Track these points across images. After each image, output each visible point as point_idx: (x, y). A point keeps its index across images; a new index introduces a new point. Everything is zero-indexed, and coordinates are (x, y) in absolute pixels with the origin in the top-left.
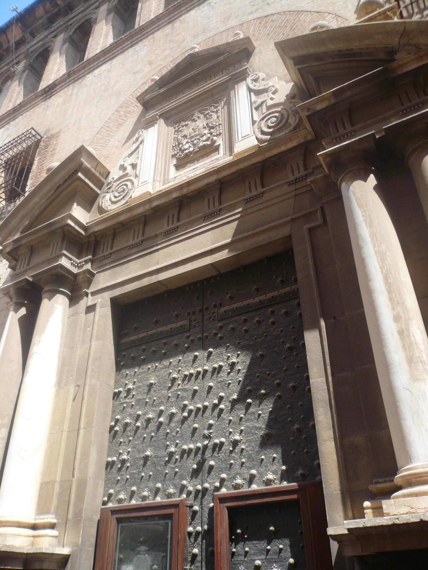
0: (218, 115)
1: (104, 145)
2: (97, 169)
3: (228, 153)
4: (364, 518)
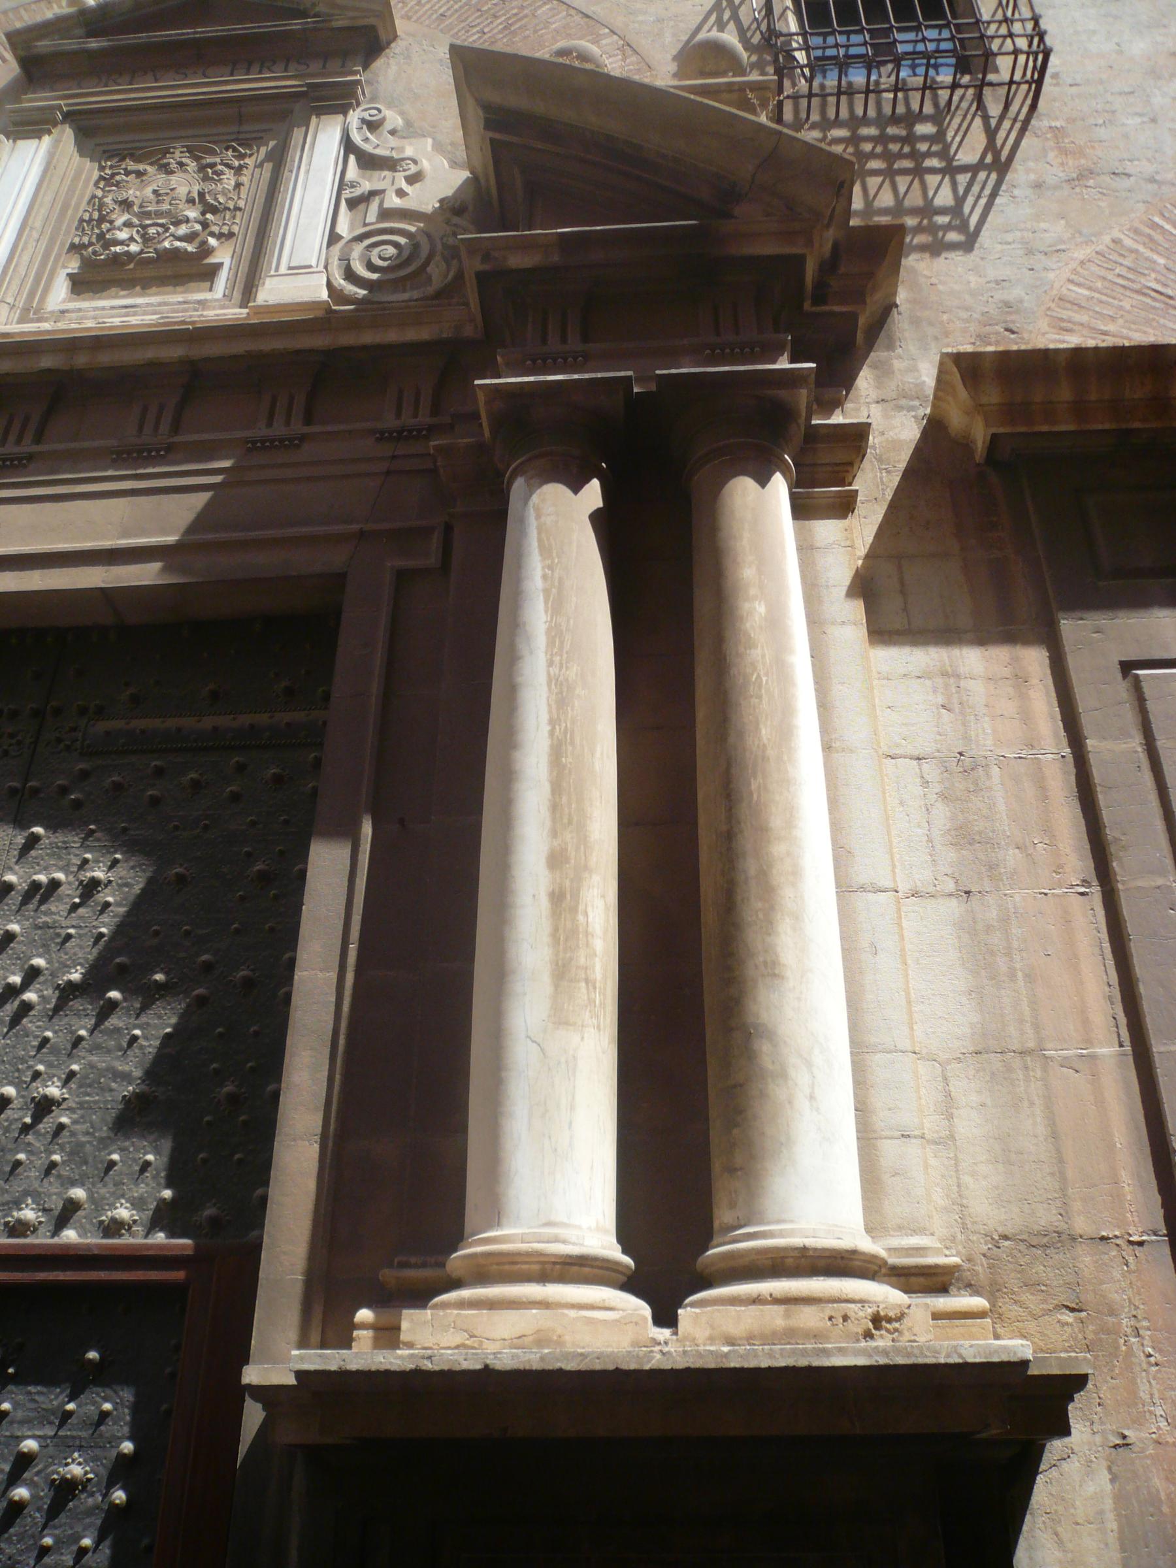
0: (239, 180)
3: (237, 296)
4: (350, 1348)
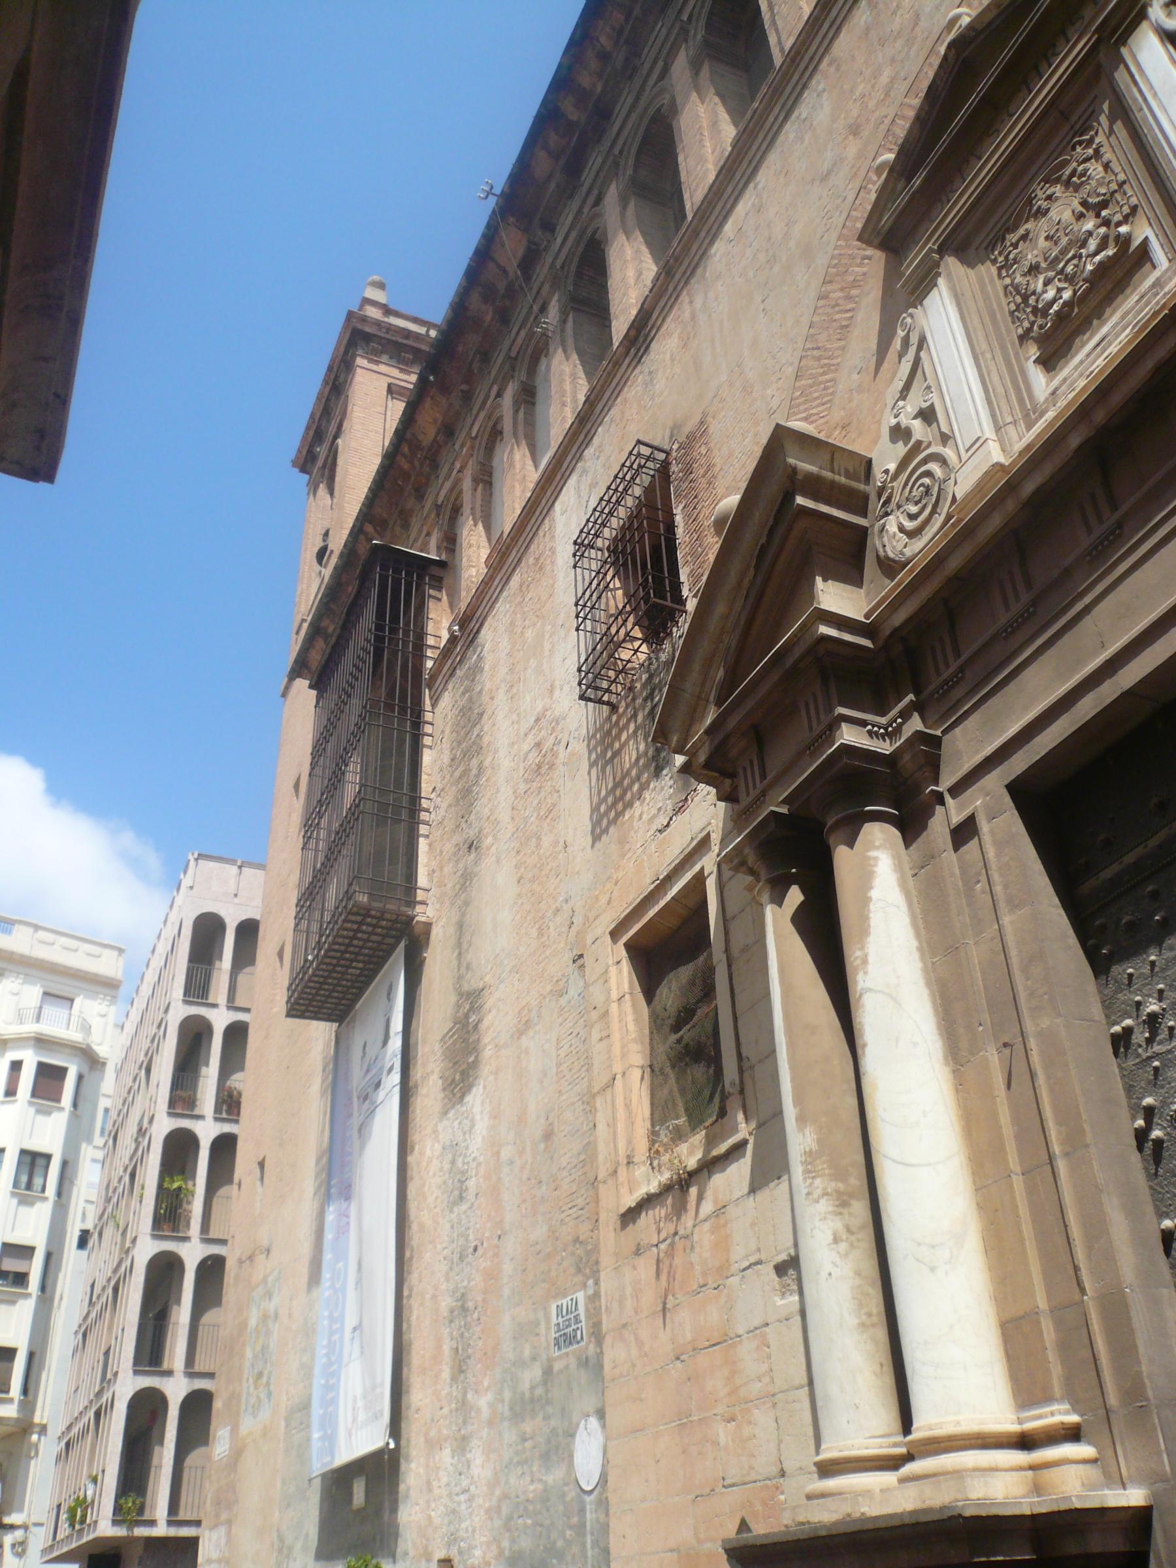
1: (825, 399)
2: (836, 468)
